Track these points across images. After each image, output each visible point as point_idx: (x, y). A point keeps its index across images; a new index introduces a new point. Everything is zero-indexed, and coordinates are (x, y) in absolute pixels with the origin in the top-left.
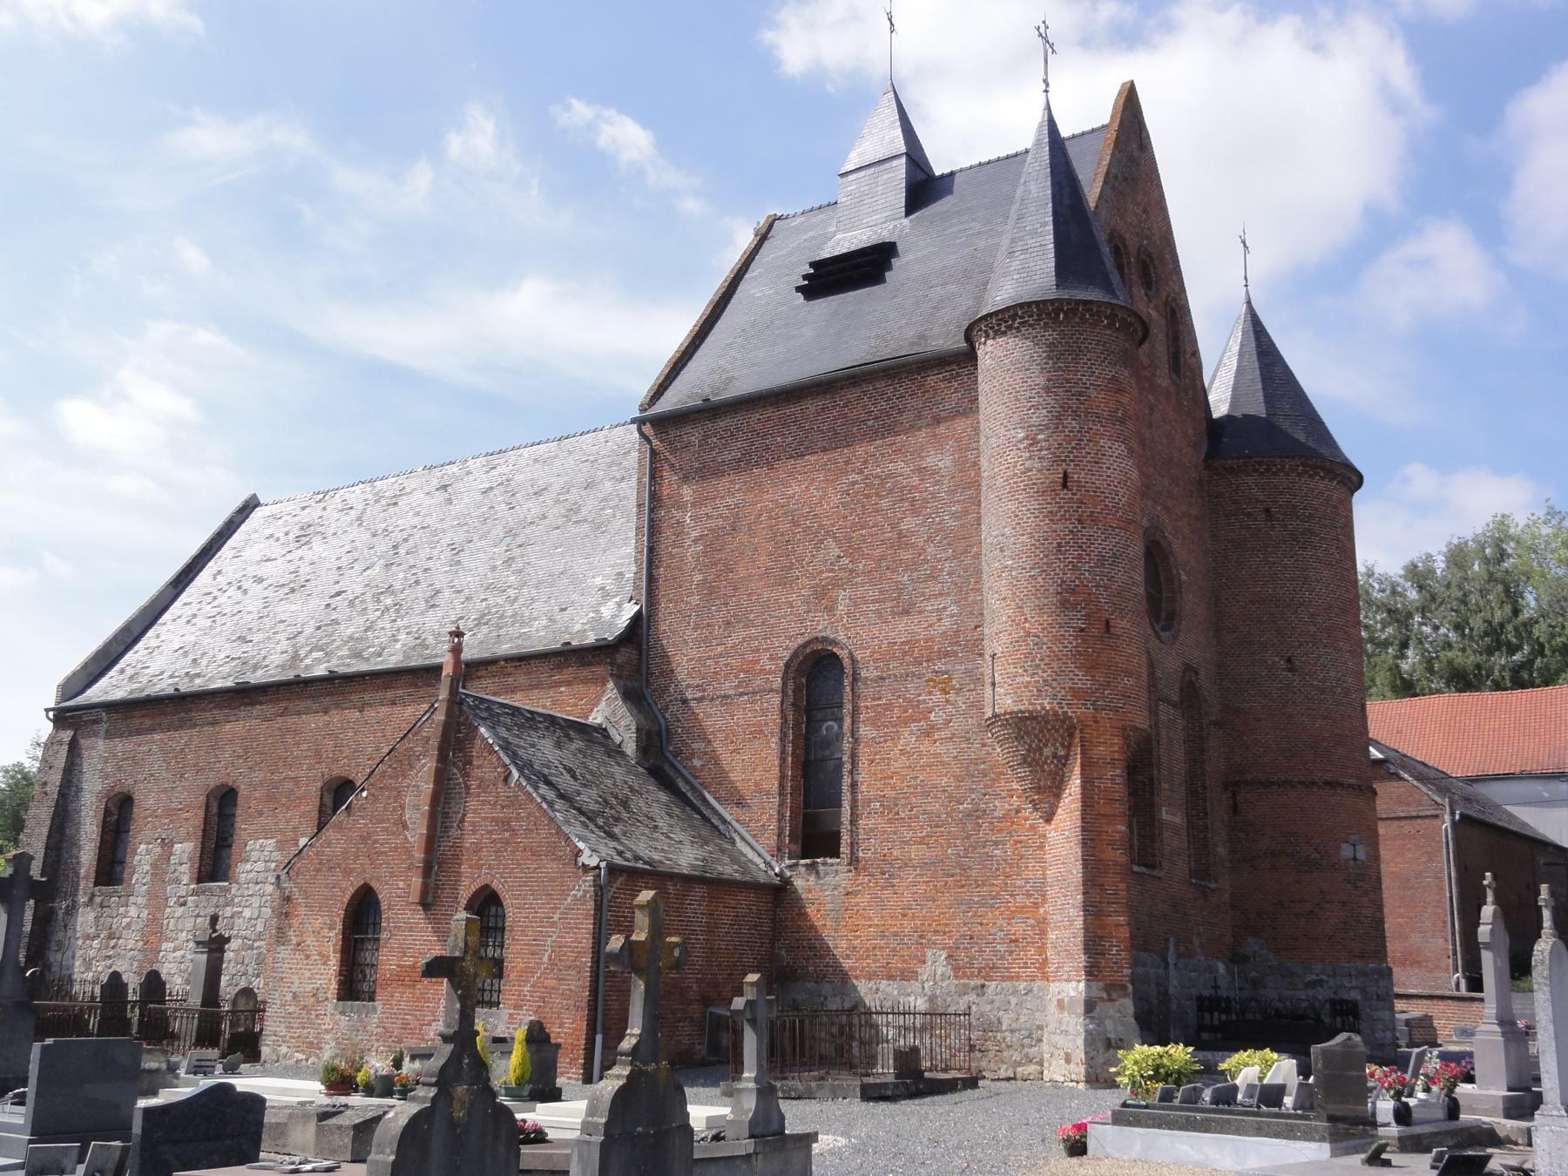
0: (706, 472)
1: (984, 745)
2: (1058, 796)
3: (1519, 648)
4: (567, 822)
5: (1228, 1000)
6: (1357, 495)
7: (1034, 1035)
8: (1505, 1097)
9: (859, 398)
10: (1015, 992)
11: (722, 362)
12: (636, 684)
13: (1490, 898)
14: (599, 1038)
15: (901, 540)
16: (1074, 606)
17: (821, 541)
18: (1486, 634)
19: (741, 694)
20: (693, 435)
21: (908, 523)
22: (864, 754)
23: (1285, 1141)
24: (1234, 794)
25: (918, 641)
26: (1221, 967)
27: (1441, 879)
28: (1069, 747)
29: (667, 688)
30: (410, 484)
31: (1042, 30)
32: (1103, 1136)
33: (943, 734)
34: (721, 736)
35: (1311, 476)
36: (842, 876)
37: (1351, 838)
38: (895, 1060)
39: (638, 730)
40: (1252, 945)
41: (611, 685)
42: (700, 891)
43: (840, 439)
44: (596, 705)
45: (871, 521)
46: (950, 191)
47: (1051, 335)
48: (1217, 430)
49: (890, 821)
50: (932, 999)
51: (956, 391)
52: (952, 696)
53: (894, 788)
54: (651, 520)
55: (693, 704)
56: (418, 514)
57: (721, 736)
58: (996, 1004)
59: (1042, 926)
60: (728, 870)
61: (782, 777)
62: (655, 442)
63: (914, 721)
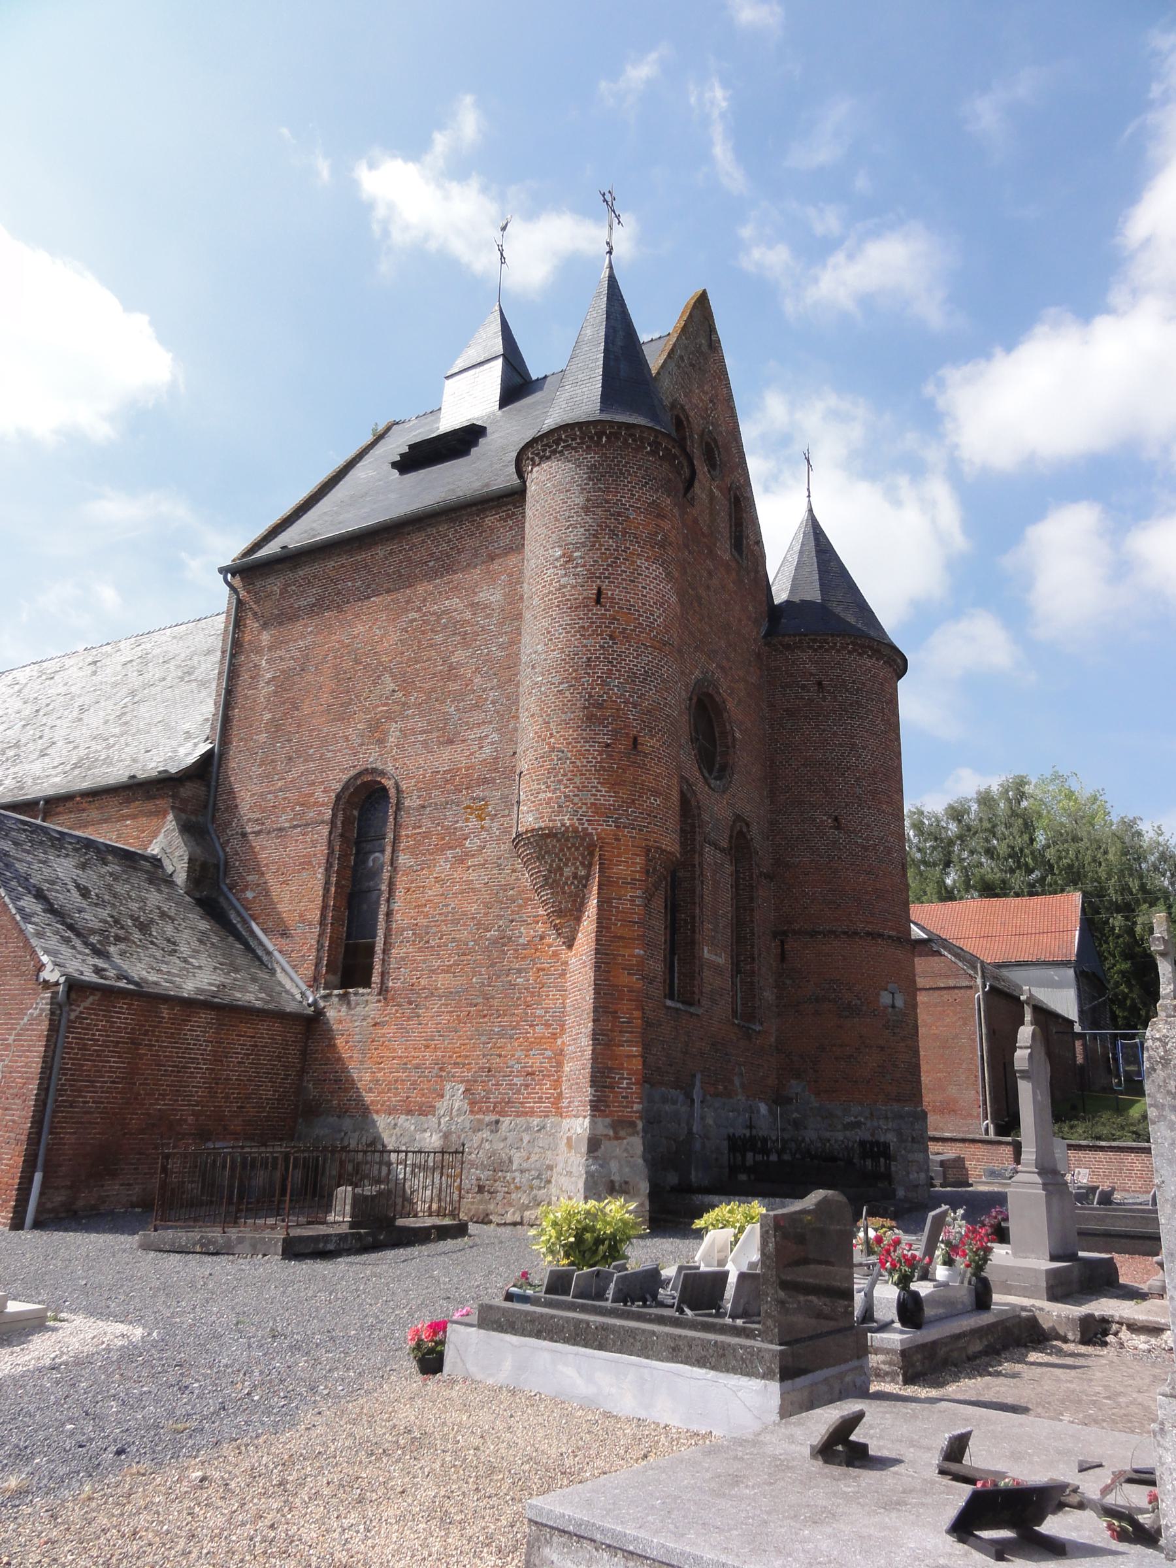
0: (282, 618)
1: (514, 871)
2: (578, 920)
3: (1032, 871)
4: (39, 935)
5: (765, 1140)
6: (901, 684)
7: (543, 1177)
8: (1051, 1273)
9: (424, 542)
10: (528, 1129)
11: (314, 525)
12: (201, 819)
13: (1028, 1017)
14: (38, 1177)
15: (452, 672)
16: (601, 721)
17: (379, 677)
18: (1010, 856)
19: (295, 827)
20: (274, 584)
21: (460, 655)
22: (401, 882)
23: (712, 1374)
24: (782, 942)
25: (459, 769)
26: (763, 1108)
27: (974, 1040)
28: (590, 866)
29: (230, 823)
30: (68, 662)
31: (608, 197)
32: (467, 1345)
33: (476, 861)
34: (273, 868)
35: (860, 654)
36: (372, 1006)
37: (890, 986)
38: (353, 1206)
39: (190, 860)
40: (795, 1087)
41: (170, 817)
42: (205, 1017)
43: (404, 580)
44: (155, 837)
45: (425, 655)
46: (541, 389)
47: (593, 458)
48: (776, 614)
49: (420, 950)
50: (446, 1136)
51: (511, 529)
52: (487, 823)
53: (426, 916)
54: (231, 664)
55: (251, 837)
56: (66, 684)
57: (273, 868)
58: (509, 1142)
59: (559, 1058)
60: (251, 996)
61: (324, 908)
62: (242, 593)
63: (451, 848)
